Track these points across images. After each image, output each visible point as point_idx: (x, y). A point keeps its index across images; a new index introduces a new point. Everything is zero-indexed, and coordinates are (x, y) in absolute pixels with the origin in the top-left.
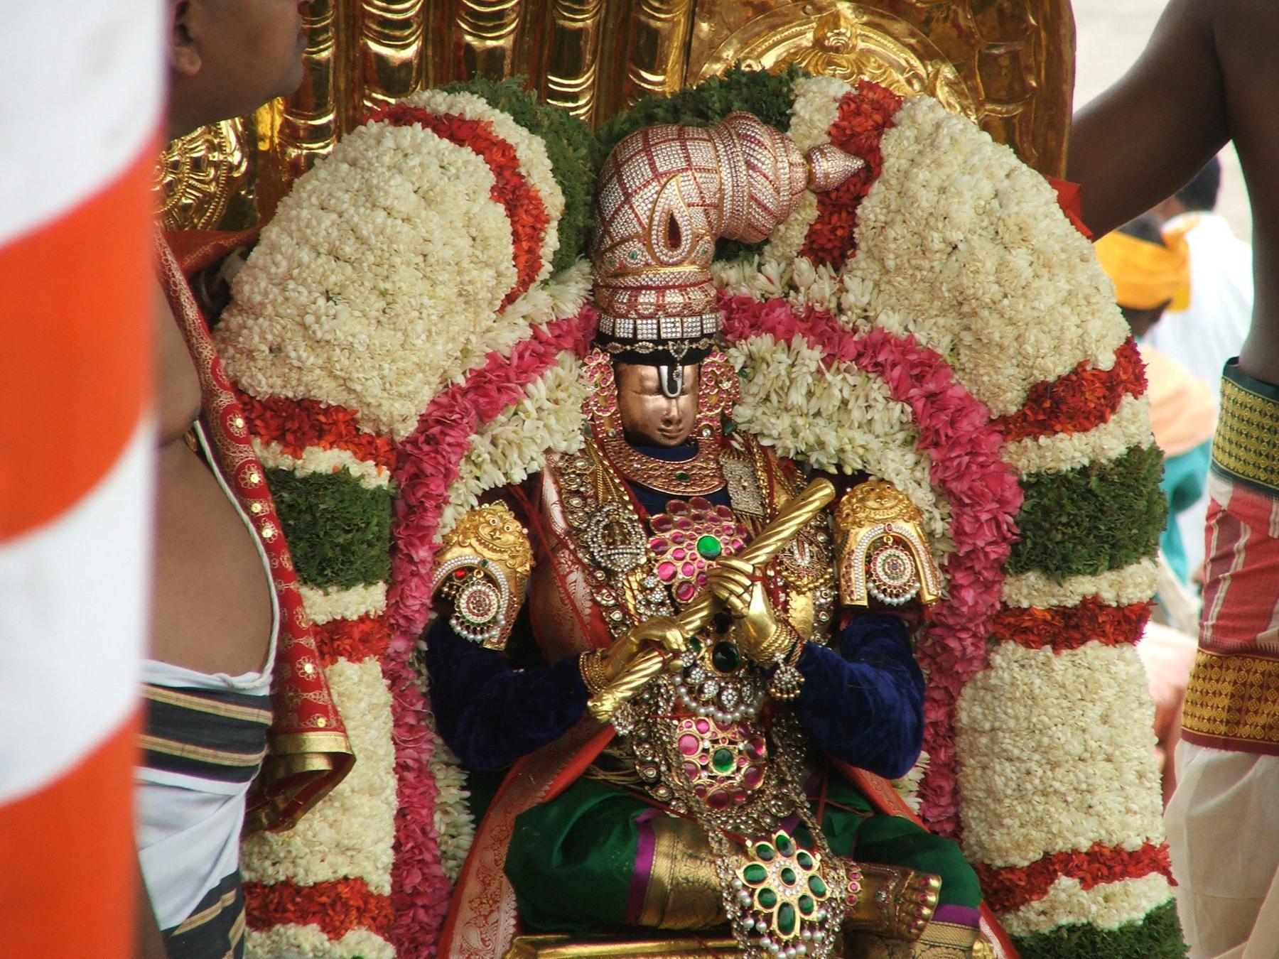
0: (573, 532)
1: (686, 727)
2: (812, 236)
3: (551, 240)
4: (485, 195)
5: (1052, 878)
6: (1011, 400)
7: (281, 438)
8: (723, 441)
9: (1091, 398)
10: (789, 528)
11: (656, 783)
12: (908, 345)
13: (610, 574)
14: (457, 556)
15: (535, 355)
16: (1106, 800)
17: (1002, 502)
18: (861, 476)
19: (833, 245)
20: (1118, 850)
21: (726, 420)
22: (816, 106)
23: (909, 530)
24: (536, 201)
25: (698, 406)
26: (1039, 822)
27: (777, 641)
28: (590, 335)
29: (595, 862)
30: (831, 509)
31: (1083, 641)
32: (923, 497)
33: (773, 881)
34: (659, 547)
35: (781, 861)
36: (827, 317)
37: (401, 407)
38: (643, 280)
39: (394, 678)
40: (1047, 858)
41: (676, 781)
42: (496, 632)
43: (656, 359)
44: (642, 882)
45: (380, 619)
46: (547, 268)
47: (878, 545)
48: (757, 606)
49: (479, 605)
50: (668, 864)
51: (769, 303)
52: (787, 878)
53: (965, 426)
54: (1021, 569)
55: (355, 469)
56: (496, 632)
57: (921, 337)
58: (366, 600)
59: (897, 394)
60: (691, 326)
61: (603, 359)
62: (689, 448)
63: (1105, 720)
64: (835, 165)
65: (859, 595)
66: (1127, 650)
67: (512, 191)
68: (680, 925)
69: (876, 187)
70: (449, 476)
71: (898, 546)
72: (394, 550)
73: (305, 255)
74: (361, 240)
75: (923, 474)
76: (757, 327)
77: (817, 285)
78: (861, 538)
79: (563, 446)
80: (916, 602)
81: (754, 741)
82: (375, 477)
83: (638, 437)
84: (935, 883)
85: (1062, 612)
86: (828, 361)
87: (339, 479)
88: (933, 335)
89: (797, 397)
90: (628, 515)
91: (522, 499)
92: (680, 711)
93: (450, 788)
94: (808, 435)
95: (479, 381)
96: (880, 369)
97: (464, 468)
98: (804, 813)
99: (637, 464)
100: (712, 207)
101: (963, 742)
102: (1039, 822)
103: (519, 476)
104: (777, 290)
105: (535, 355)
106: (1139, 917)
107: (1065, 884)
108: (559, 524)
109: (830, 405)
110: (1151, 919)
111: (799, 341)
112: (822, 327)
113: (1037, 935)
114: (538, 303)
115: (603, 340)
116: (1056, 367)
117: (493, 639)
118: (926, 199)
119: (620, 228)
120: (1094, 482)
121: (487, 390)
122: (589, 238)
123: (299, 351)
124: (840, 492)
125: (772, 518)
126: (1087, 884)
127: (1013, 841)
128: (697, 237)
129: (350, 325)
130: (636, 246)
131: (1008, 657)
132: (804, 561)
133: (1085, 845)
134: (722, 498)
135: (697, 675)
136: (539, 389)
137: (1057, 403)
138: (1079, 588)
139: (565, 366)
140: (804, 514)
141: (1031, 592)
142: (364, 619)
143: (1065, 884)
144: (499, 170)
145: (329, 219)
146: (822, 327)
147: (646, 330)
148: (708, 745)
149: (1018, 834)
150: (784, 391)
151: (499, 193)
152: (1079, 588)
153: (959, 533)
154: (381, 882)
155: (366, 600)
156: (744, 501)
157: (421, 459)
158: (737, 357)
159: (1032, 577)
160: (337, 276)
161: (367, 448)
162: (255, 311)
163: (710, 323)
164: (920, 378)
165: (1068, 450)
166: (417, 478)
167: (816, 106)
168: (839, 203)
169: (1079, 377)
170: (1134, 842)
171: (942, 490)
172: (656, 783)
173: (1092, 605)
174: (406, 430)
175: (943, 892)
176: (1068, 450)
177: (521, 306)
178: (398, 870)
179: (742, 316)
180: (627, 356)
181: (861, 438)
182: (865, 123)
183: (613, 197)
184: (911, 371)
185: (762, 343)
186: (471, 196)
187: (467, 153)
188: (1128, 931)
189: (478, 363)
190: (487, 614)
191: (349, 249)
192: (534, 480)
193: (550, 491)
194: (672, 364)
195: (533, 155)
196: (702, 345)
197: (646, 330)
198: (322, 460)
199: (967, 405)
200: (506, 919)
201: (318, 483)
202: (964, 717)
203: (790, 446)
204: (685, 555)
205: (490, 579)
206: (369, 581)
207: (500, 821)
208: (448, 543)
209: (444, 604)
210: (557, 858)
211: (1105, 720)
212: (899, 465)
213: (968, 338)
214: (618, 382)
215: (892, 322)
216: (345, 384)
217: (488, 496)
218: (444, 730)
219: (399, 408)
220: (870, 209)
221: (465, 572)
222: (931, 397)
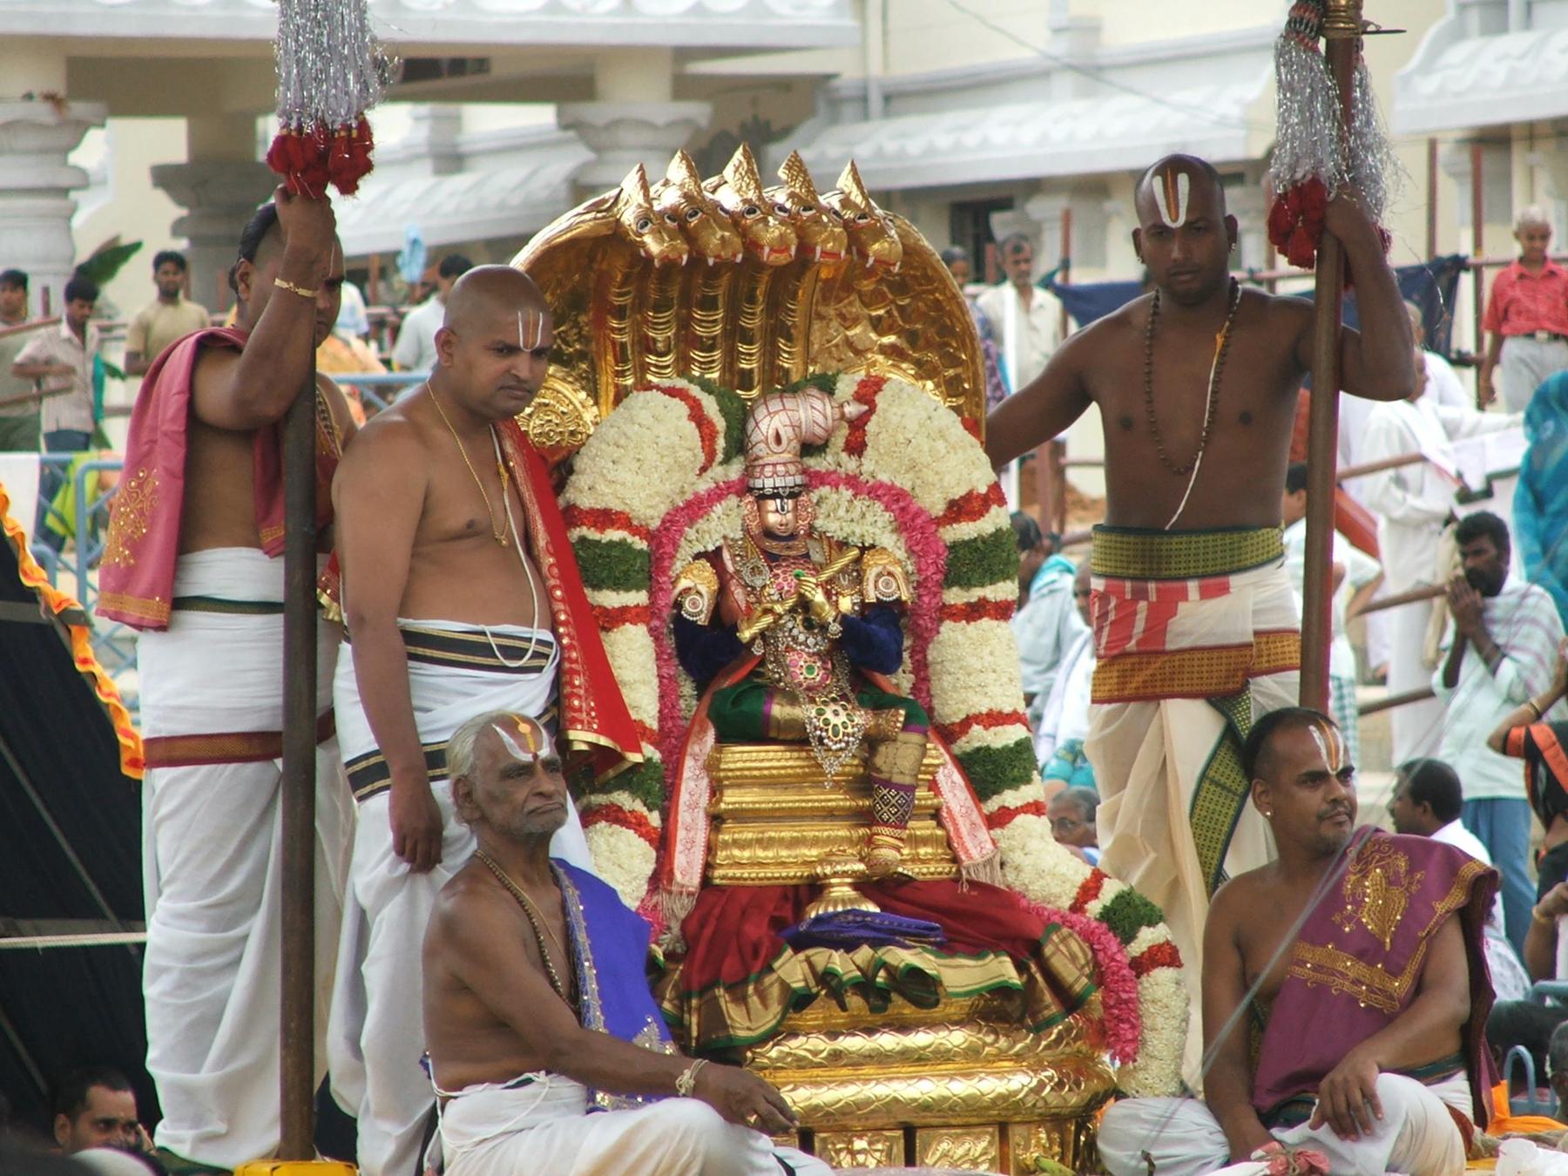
0: (737, 572)
1: (791, 657)
2: (847, 443)
3: (721, 443)
4: (685, 418)
5: (970, 726)
6: (938, 509)
7: (595, 526)
8: (809, 535)
9: (976, 505)
10: (837, 566)
11: (780, 680)
12: (892, 487)
13: (754, 588)
14: (684, 583)
15: (718, 494)
16: (994, 690)
17: (938, 555)
18: (873, 546)
19: (856, 447)
20: (1000, 713)
21: (811, 527)
22: (846, 386)
23: (898, 570)
24: (710, 424)
25: (796, 518)
26: (963, 702)
27: (829, 614)
28: (743, 488)
29: (745, 707)
30: (858, 560)
31: (981, 617)
32: (901, 554)
33: (829, 715)
34: (776, 576)
35: (833, 707)
36: (855, 477)
37: (651, 511)
38: (766, 460)
39: (652, 631)
40: (968, 717)
41: (788, 679)
42: (703, 616)
43: (774, 496)
44: (767, 717)
45: (646, 608)
46: (720, 456)
47: (879, 575)
48: (819, 597)
49: (694, 604)
50: (778, 710)
51: (829, 473)
52: (836, 713)
53: (919, 521)
54: (950, 586)
55: (630, 539)
56: (703, 616)
57: (898, 484)
58: (639, 598)
59: (887, 509)
60: (790, 481)
61: (751, 499)
62: (793, 536)
63: (991, 654)
64: (852, 410)
65: (871, 597)
66: (1002, 624)
67: (697, 415)
68: (790, 737)
69: (874, 418)
70: (676, 546)
71: (890, 577)
72: (650, 578)
73: (603, 446)
74: (628, 438)
75: (901, 544)
76: (823, 484)
77: (850, 464)
78: (871, 575)
79: (732, 535)
80: (898, 600)
81: (824, 662)
82: (640, 544)
83: (769, 533)
84: (902, 712)
85: (968, 604)
86: (855, 496)
87: (622, 543)
88: (904, 482)
89: (841, 512)
90: (762, 563)
91: (714, 557)
92: (788, 649)
93: (687, 688)
94: (847, 530)
95: (689, 504)
96: (878, 497)
97: (683, 542)
98: (848, 691)
99: (768, 544)
100: (796, 427)
101: (930, 670)
102: (963, 702)
103: (711, 548)
104: (832, 468)
105: (718, 494)
106: (1011, 743)
107: (976, 729)
108: (731, 568)
109: (856, 514)
110: (1018, 744)
111: (842, 488)
112: (853, 482)
113: (966, 754)
114: (717, 472)
115: (750, 490)
116: (959, 492)
117: (702, 620)
118: (895, 420)
119: (754, 439)
120: (980, 544)
121: (695, 508)
122: (739, 445)
123: (602, 487)
124: (862, 553)
125: (830, 562)
126: (986, 728)
127: (951, 708)
128: (790, 441)
129: (625, 474)
130: (762, 445)
131: (948, 629)
132: (845, 583)
133: (984, 710)
134: (807, 556)
135: (795, 632)
136: (718, 509)
137: (960, 508)
138: (975, 594)
139: (732, 500)
140: (845, 560)
141: (955, 596)
142: (637, 606)
143: (976, 729)
144: (692, 408)
145: (613, 431)
146: (853, 482)
147: (769, 483)
148: (803, 663)
149: (955, 708)
150: (835, 510)
151: (692, 417)
152: (975, 594)
153: (920, 571)
154: (654, 725)
155: (639, 598)
156: (817, 557)
157: (664, 538)
158: (814, 497)
159: (955, 589)
160: (617, 453)
161: (636, 531)
162: (582, 473)
163: (799, 479)
164: (898, 501)
165: (965, 530)
166: (660, 545)
167: (846, 386)
168: (858, 425)
169: (969, 497)
170: (1007, 709)
171: (910, 551)
172: (780, 680)
173: (983, 602)
174: (655, 524)
175: (907, 717)
176: (965, 530)
177: (709, 473)
178: (662, 718)
179: (815, 479)
180: (762, 497)
181: (871, 530)
182: (868, 392)
183: (751, 425)
184: (896, 500)
185: (825, 490)
186: (679, 418)
187: (677, 400)
188: (1006, 749)
189: (689, 496)
190: (698, 609)
191: (622, 442)
192: (719, 550)
193: (726, 555)
194: (782, 498)
195: (710, 405)
196: (796, 490)
197: (769, 483)
198: (614, 535)
199: (920, 512)
200: (710, 737)
201: (611, 544)
202: (930, 658)
203: (840, 535)
204: (786, 580)
205: (698, 593)
206: (638, 589)
207: (707, 699)
208: (678, 577)
209: (678, 605)
210: (729, 706)
211: (991, 654)
212: (889, 540)
213: (918, 482)
214: (759, 509)
215: (884, 477)
216: (623, 500)
217: (698, 556)
218: (683, 662)
219: (650, 512)
220: (871, 427)
221: (687, 590)
222: (902, 509)
